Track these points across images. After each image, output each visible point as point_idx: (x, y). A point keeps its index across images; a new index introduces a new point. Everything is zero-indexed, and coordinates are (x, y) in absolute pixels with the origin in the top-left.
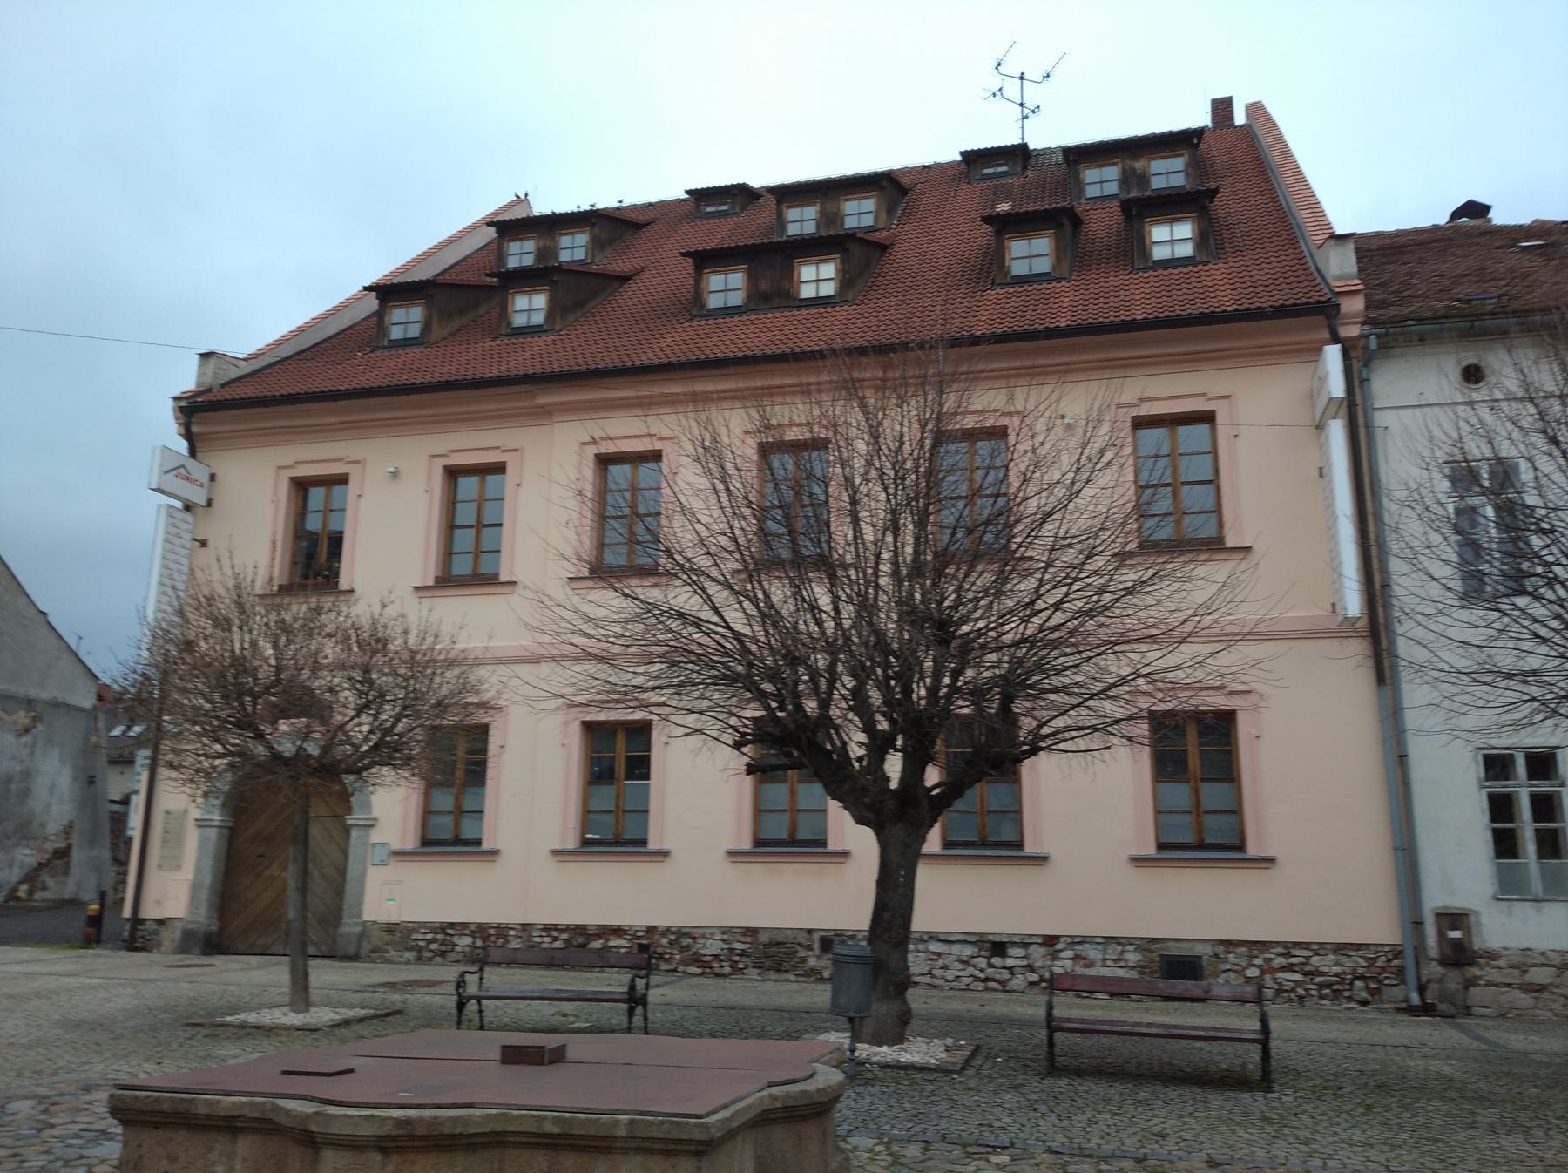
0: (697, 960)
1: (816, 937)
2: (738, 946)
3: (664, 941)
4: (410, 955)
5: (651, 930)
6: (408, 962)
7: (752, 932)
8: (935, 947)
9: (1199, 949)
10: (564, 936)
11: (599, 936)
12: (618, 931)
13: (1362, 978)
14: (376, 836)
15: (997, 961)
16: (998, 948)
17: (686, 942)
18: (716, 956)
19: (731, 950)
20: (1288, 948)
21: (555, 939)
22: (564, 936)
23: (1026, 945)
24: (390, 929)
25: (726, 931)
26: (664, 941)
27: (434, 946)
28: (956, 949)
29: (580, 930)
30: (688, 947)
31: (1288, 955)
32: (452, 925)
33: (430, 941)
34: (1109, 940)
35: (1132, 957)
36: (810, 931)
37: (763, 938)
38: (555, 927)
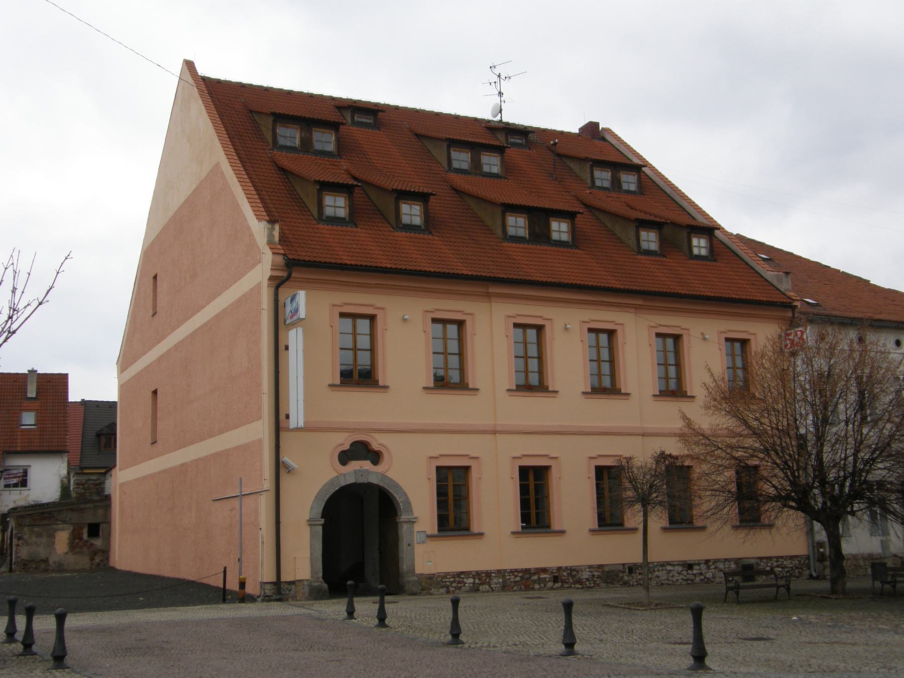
0: (579, 582)
1: (626, 566)
2: (596, 573)
3: (565, 574)
4: (443, 590)
5: (559, 569)
6: (442, 594)
7: (600, 566)
8: (669, 568)
9: (753, 561)
10: (520, 574)
11: (535, 574)
12: (544, 570)
13: (797, 568)
14: (417, 528)
15: (690, 572)
16: (690, 566)
17: (574, 573)
18: (587, 579)
19: (593, 576)
20: (778, 558)
21: (516, 576)
22: (520, 574)
23: (699, 564)
24: (431, 577)
25: (591, 567)
26: (565, 574)
27: (454, 585)
28: (676, 567)
29: (527, 571)
30: (575, 576)
31: (777, 561)
32: (462, 573)
33: (451, 583)
34: (726, 560)
35: (733, 566)
36: (624, 564)
37: (606, 569)
38: (516, 571)
